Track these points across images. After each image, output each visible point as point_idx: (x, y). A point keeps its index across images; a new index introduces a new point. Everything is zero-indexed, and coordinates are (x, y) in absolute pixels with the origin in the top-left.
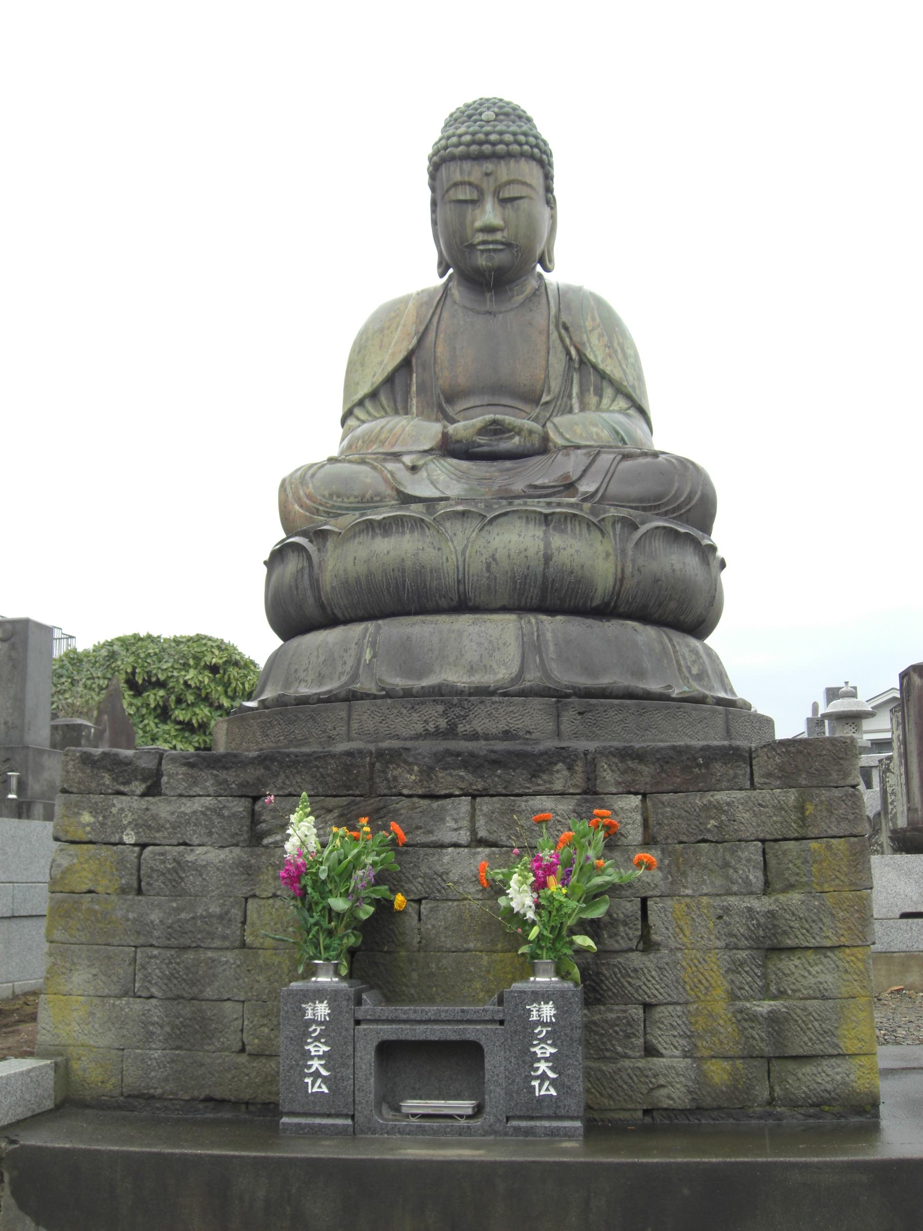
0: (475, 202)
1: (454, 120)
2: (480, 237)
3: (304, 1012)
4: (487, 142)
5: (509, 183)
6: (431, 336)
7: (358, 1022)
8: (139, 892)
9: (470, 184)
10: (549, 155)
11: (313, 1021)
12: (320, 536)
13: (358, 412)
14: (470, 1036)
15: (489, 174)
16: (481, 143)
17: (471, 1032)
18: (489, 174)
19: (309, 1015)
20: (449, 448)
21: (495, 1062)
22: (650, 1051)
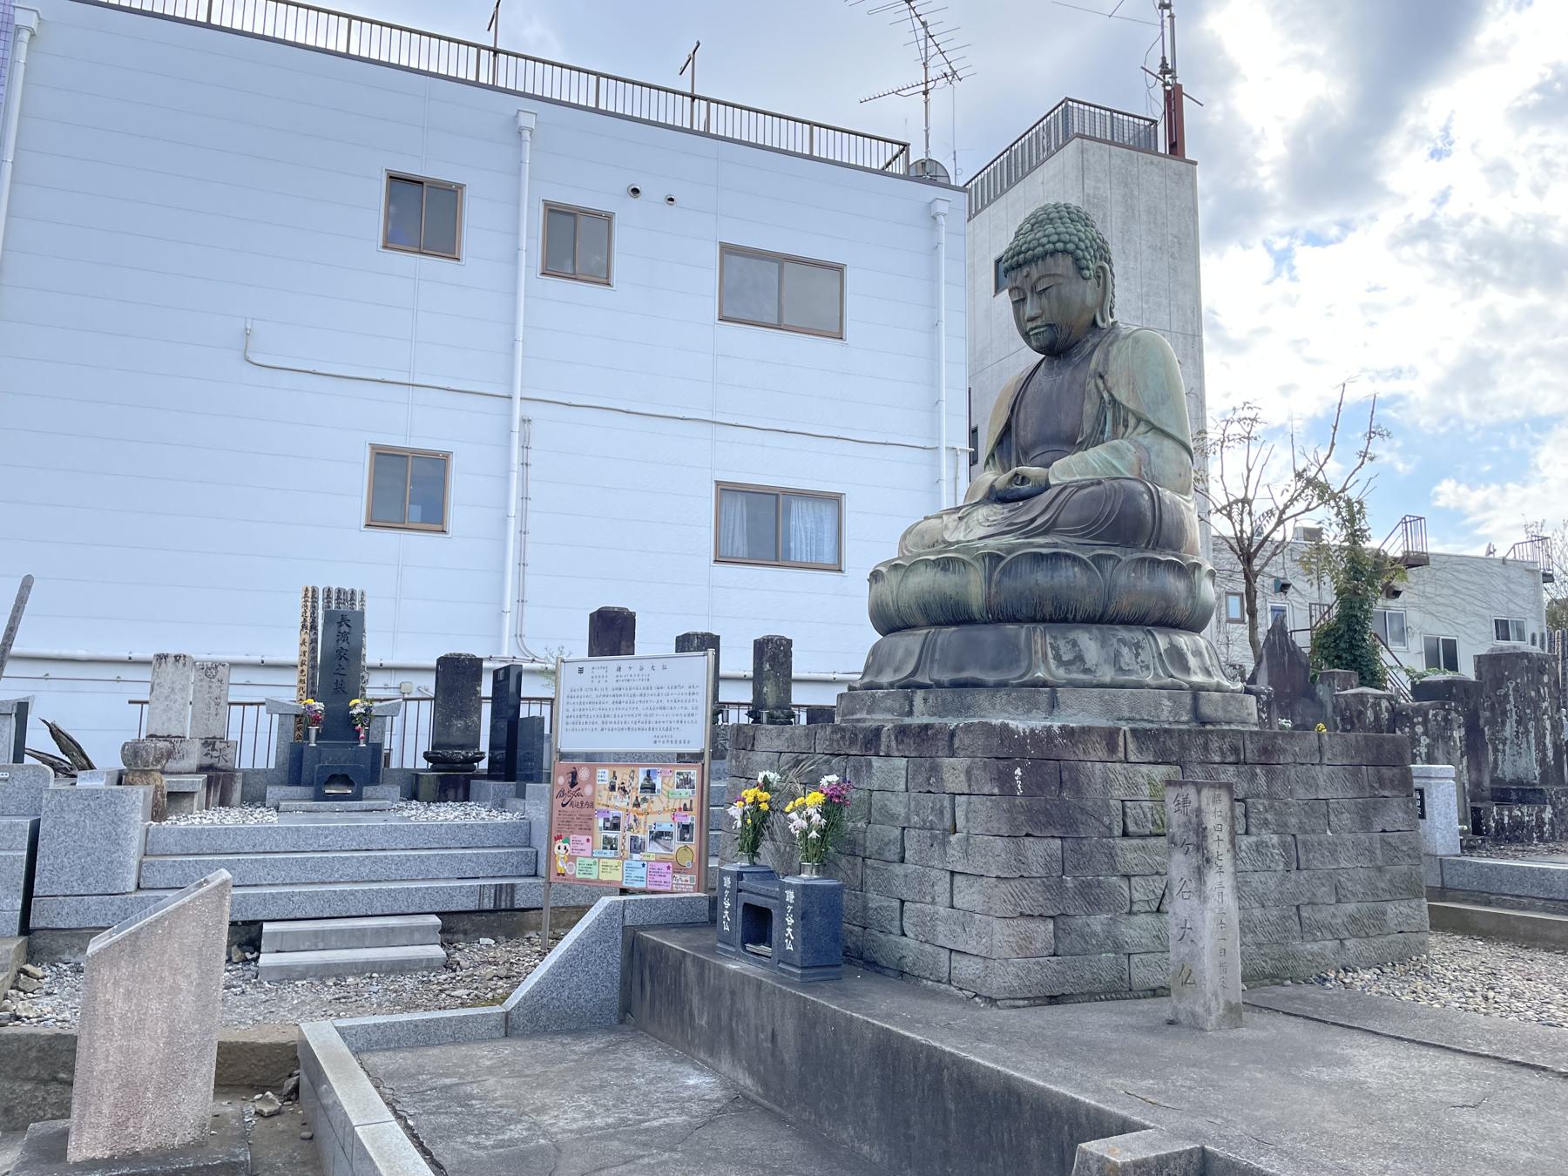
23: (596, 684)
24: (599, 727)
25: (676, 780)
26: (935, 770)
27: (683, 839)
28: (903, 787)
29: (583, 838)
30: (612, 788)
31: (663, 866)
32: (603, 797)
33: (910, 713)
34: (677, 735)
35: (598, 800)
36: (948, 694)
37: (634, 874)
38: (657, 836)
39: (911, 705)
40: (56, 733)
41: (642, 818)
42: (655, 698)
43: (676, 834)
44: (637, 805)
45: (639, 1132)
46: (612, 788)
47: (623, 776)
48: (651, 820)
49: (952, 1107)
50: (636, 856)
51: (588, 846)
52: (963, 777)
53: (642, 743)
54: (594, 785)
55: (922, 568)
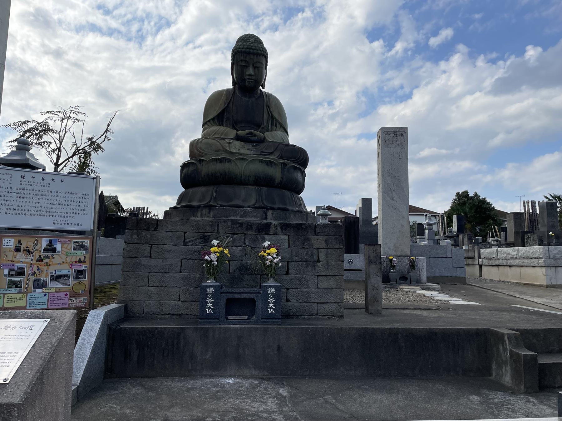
0: (247, 67)
2: (247, 77)
3: (206, 291)
4: (252, 49)
5: (257, 62)
6: (231, 105)
7: (221, 293)
8: (151, 257)
9: (246, 61)
10: (267, 54)
11: (209, 293)
12: (200, 161)
13: (208, 123)
15: (249, 57)
16: (250, 49)
17: (252, 296)
18: (249, 57)
20: (238, 138)
21: (258, 304)
22: (288, 301)
25: (73, 246)
26: (307, 240)
27: (77, 278)
28: (287, 245)
30: (18, 250)
31: (62, 295)
33: (266, 218)
34: (71, 220)
36: (281, 213)
38: (56, 278)
39: (266, 216)
40: (74, 131)
43: (73, 275)
45: (262, 402)
46: (18, 250)
48: (52, 269)
49: (403, 345)
50: (38, 291)
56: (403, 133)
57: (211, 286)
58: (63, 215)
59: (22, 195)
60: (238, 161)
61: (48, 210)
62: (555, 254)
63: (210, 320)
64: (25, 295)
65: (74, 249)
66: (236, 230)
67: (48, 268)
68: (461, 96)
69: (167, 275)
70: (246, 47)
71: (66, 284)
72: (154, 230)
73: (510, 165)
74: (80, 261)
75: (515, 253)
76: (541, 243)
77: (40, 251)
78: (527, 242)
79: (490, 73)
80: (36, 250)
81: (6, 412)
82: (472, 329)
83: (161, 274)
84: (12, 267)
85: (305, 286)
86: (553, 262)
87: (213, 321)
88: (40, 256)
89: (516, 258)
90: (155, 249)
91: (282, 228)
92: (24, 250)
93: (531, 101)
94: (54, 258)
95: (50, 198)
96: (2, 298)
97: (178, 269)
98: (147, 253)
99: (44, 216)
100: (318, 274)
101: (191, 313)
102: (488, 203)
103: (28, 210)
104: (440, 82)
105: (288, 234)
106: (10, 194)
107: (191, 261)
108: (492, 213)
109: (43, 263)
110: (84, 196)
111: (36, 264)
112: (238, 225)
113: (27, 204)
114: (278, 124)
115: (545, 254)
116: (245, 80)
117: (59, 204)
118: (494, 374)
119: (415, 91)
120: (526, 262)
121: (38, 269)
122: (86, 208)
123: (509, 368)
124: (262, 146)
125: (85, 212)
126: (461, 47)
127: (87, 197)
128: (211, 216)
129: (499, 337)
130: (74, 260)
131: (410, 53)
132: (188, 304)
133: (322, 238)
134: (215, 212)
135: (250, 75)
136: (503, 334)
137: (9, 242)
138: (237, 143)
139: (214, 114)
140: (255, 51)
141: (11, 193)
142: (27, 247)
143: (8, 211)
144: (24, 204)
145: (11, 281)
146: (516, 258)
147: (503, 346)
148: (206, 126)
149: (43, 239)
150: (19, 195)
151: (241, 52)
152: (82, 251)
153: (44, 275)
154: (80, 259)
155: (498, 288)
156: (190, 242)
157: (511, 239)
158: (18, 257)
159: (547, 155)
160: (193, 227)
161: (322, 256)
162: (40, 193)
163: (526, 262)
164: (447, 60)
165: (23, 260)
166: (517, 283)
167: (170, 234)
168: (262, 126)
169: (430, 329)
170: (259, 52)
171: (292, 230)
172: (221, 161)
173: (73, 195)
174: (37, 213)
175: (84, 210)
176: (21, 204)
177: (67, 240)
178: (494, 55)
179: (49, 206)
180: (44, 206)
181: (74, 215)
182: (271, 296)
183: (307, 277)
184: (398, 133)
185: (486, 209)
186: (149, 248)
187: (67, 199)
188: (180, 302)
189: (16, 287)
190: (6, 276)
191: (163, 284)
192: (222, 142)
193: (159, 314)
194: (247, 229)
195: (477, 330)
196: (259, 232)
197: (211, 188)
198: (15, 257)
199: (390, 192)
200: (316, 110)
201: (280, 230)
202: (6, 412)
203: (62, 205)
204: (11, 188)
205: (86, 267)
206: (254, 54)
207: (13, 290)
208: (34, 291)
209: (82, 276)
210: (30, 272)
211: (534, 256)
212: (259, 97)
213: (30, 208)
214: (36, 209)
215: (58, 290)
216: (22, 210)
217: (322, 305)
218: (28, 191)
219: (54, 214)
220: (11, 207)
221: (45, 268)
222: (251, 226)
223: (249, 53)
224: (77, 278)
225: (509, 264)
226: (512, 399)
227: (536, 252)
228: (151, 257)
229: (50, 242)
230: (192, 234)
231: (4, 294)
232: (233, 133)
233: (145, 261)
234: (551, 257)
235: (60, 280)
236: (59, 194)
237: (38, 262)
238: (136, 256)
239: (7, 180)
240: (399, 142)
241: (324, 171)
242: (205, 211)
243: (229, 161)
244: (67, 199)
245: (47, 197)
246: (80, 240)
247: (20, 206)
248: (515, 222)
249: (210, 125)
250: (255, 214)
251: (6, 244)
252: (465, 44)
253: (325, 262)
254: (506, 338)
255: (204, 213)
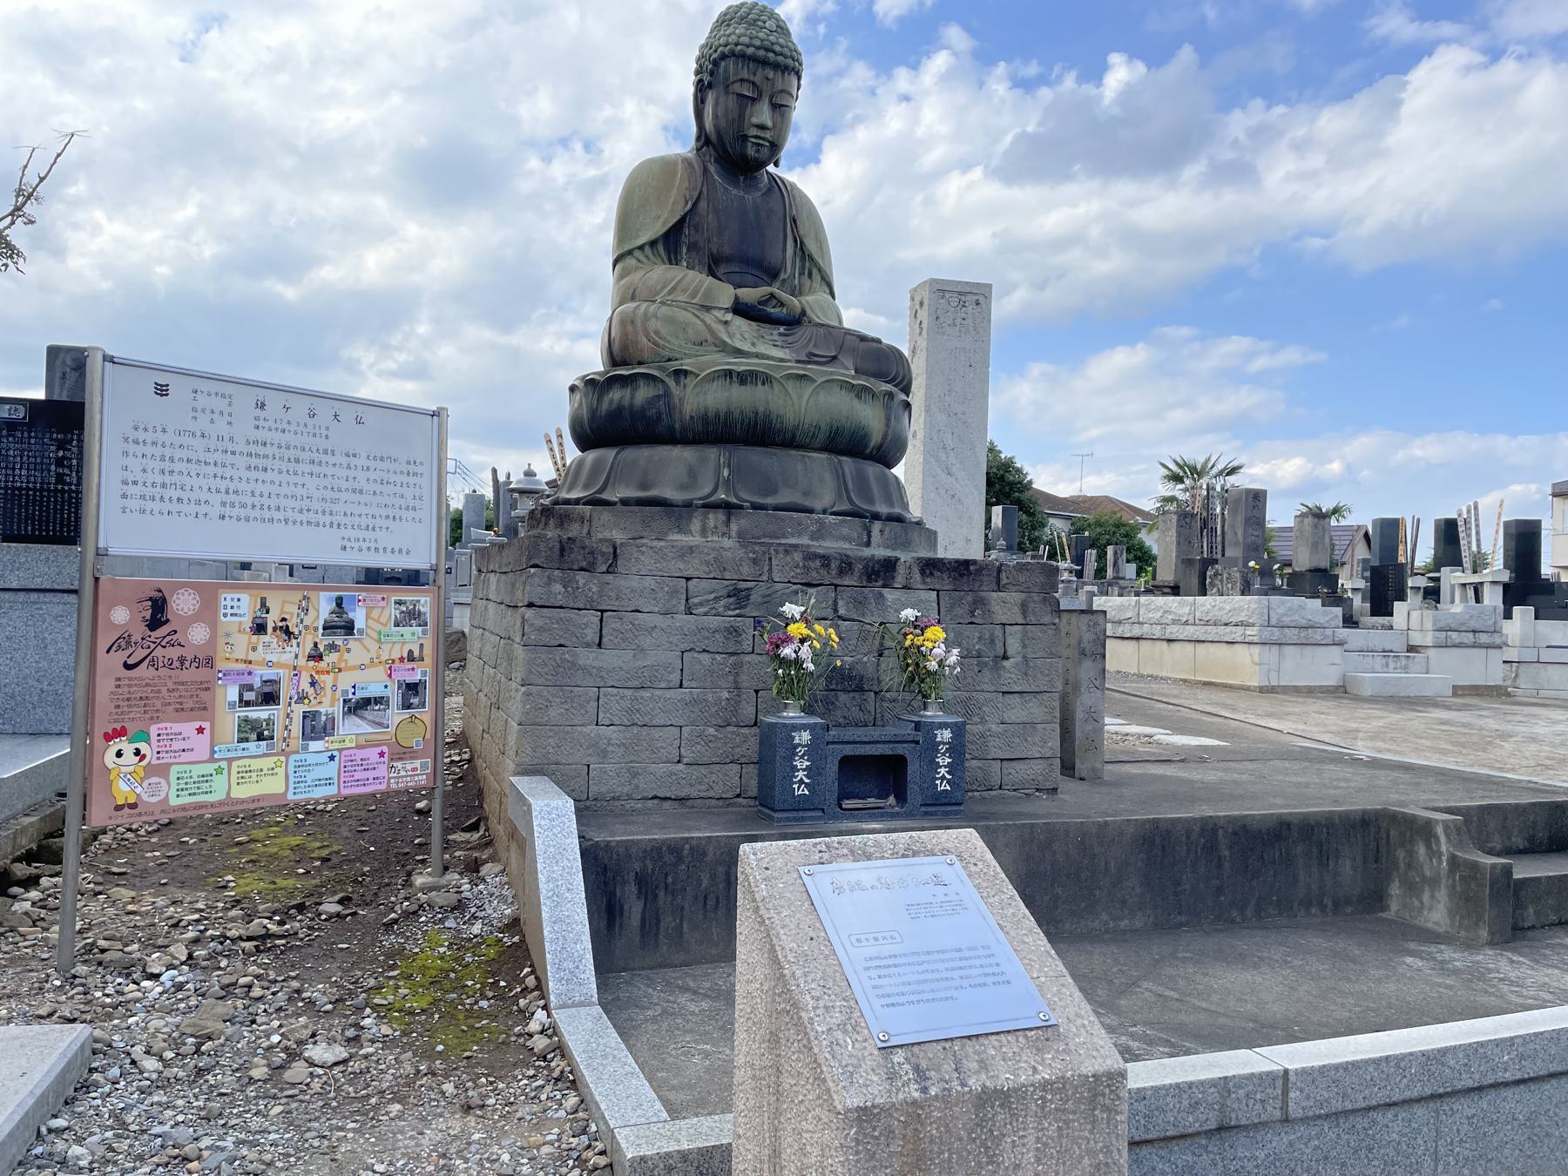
1: (725, 20)
2: (753, 131)
5: (782, 91)
6: (703, 205)
9: (754, 84)
14: (900, 752)
16: (767, 50)
17: (900, 750)
19: (797, 741)
20: (740, 309)
21: (913, 769)
23: (202, 424)
24: (215, 511)
25: (394, 612)
26: (980, 602)
27: (407, 706)
29: (189, 728)
30: (260, 628)
31: (372, 754)
32: (237, 646)
33: (868, 544)
34: (383, 539)
35: (222, 652)
37: (310, 777)
38: (358, 707)
39: (869, 536)
41: (327, 680)
42: (343, 473)
44: (316, 657)
46: (260, 628)
47: (281, 607)
48: (345, 681)
50: (315, 745)
51: (201, 744)
52: (1016, 609)
53: (320, 547)
54: (213, 625)
55: (836, 389)
56: (981, 299)
57: (804, 727)
58: (364, 521)
59: (261, 463)
60: (791, 383)
61: (328, 506)
62: (1283, 615)
63: (801, 814)
64: (283, 759)
65: (397, 625)
66: (814, 574)
67: (335, 679)
68: (940, 173)
69: (646, 694)
70: (758, 43)
71: (380, 725)
72: (608, 572)
73: (1036, 369)
74: (411, 658)
75: (1187, 610)
76: (1246, 590)
77: (316, 629)
78: (1213, 585)
79: (1011, 111)
80: (306, 628)
81: (1107, 1091)
82: (1355, 811)
83: (630, 692)
84: (247, 680)
85: (976, 719)
86: (1276, 634)
87: (809, 814)
88: (316, 644)
89: (1186, 623)
90: (611, 622)
91: (922, 572)
92: (275, 629)
93: (1095, 206)
94: (348, 651)
95: (330, 471)
96: (225, 772)
97: (675, 678)
98: (591, 634)
99: (318, 524)
100: (1005, 689)
101: (711, 794)
102: (1019, 471)
103: (279, 508)
104: (895, 121)
105: (937, 587)
106: (229, 459)
107: (706, 656)
108: (1027, 495)
109: (322, 665)
110: (412, 468)
111: (306, 668)
112: (818, 563)
113: (275, 489)
114: (815, 271)
115: (1262, 614)
116: (745, 138)
117: (354, 491)
118: (1394, 906)
119: (828, 142)
120: (1213, 632)
121: (313, 684)
122: (417, 503)
123: (1442, 895)
124: (802, 333)
125: (417, 515)
126: (955, 34)
127: (419, 469)
128: (733, 534)
129: (1424, 830)
130: (396, 655)
131: (822, 29)
132: (702, 769)
133: (1014, 597)
134: (743, 522)
135: (762, 127)
136: (1429, 823)
137: (235, 603)
138: (740, 323)
139: (655, 227)
140: (780, 58)
141: (233, 453)
142: (284, 620)
143: (227, 511)
144: (266, 489)
145: (246, 720)
146: (1186, 623)
147: (1429, 847)
148: (630, 261)
149: (322, 594)
150: (254, 461)
151: (743, 56)
152: (414, 628)
153: (327, 700)
154: (410, 652)
155: (1166, 696)
156: (701, 604)
157: (1166, 572)
158: (260, 648)
159: (1120, 348)
160: (708, 563)
161: (1014, 646)
162: (306, 456)
163: (1213, 632)
164: (915, 67)
165: (274, 658)
166: (1185, 681)
167: (650, 582)
168: (783, 276)
169: (1280, 816)
170: (790, 61)
171: (945, 576)
172: (745, 378)
173: (386, 465)
174: (299, 517)
175: (414, 509)
176: (259, 488)
177: (379, 597)
178: (1033, 70)
179: (329, 495)
180: (317, 495)
181: (390, 523)
182: (942, 748)
183: (981, 696)
184: (969, 297)
185: (1011, 484)
186: (597, 620)
187: (372, 475)
188: (681, 767)
189: (260, 738)
190: (232, 705)
191: (638, 719)
192: (708, 318)
193: (630, 797)
194: (841, 572)
195: (1364, 812)
196: (869, 579)
197: (712, 452)
198: (254, 649)
199: (942, 455)
200: (548, 160)
201: (918, 576)
202: (1107, 1091)
203: (361, 492)
204: (231, 439)
205: (424, 673)
206: (776, 66)
207: (252, 746)
208: (305, 748)
209: (415, 701)
210: (293, 692)
211: (1234, 620)
212: (770, 190)
213: (283, 502)
214: (297, 504)
215: (362, 740)
216: (262, 508)
217: (1014, 764)
218: (275, 449)
219: (344, 520)
220: (233, 497)
221: (327, 680)
222: (850, 564)
223: (764, 63)
224: (407, 706)
225: (1168, 636)
226: (1456, 955)
227: (1241, 609)
228: (599, 645)
229: (339, 602)
230: (705, 584)
231: (230, 760)
232: (725, 294)
233: (587, 657)
234: (1273, 622)
235: (366, 714)
236: (353, 461)
237: (312, 663)
238: (562, 642)
239: (221, 413)
240: (969, 322)
241: (561, 347)
242: (715, 518)
243: (767, 379)
244: (372, 475)
245: (324, 470)
246: (409, 595)
247: (188, 488)
248: (1179, 534)
249: (642, 257)
250: (845, 531)
251: (229, 611)
252: (967, 28)
253: (1019, 659)
254: (1440, 830)
255: (711, 523)
